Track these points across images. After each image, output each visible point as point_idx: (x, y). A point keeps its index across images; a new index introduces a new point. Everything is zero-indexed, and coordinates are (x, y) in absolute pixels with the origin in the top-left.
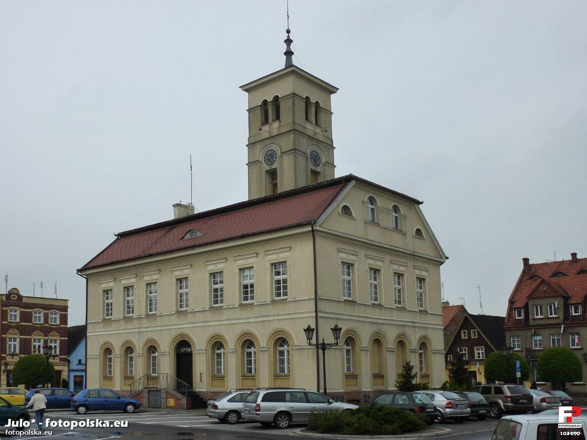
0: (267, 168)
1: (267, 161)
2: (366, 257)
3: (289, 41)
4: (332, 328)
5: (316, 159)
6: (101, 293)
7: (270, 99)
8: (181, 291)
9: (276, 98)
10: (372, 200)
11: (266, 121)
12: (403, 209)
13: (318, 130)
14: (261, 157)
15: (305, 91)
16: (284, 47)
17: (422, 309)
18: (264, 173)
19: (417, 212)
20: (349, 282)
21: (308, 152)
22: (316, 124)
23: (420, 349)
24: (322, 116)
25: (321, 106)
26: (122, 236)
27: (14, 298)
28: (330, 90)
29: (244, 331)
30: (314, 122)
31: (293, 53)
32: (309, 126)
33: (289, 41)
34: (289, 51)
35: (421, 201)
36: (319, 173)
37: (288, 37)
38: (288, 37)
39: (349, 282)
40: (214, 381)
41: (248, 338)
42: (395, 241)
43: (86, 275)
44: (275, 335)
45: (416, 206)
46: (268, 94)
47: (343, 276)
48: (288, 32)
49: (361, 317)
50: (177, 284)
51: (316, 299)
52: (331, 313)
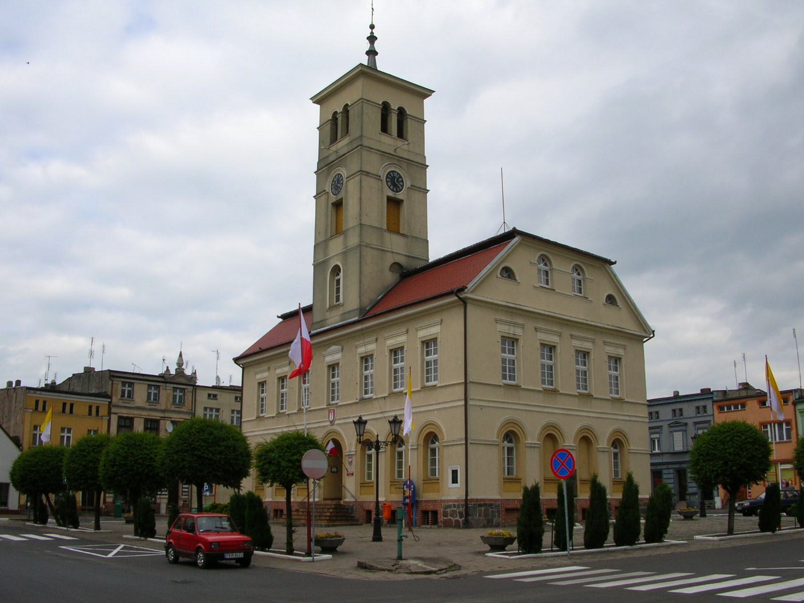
2: (497, 323)
3: (372, 39)
4: (390, 420)
5: (395, 181)
7: (340, 110)
8: (333, 380)
9: (346, 109)
10: (544, 259)
11: (334, 139)
12: (588, 273)
14: (328, 188)
16: (367, 46)
17: (617, 396)
18: (330, 205)
19: (609, 274)
20: (551, 368)
24: (410, 125)
25: (408, 113)
27: (14, 390)
29: (513, 419)
31: (376, 53)
33: (372, 39)
34: (372, 51)
35: (613, 261)
36: (402, 201)
37: (372, 33)
38: (372, 33)
39: (551, 368)
40: (299, 490)
41: (432, 430)
43: (242, 364)
44: (507, 426)
45: (607, 266)
46: (337, 106)
47: (577, 366)
48: (372, 27)
49: (484, 401)
50: (329, 371)
51: (466, 383)
52: (452, 401)
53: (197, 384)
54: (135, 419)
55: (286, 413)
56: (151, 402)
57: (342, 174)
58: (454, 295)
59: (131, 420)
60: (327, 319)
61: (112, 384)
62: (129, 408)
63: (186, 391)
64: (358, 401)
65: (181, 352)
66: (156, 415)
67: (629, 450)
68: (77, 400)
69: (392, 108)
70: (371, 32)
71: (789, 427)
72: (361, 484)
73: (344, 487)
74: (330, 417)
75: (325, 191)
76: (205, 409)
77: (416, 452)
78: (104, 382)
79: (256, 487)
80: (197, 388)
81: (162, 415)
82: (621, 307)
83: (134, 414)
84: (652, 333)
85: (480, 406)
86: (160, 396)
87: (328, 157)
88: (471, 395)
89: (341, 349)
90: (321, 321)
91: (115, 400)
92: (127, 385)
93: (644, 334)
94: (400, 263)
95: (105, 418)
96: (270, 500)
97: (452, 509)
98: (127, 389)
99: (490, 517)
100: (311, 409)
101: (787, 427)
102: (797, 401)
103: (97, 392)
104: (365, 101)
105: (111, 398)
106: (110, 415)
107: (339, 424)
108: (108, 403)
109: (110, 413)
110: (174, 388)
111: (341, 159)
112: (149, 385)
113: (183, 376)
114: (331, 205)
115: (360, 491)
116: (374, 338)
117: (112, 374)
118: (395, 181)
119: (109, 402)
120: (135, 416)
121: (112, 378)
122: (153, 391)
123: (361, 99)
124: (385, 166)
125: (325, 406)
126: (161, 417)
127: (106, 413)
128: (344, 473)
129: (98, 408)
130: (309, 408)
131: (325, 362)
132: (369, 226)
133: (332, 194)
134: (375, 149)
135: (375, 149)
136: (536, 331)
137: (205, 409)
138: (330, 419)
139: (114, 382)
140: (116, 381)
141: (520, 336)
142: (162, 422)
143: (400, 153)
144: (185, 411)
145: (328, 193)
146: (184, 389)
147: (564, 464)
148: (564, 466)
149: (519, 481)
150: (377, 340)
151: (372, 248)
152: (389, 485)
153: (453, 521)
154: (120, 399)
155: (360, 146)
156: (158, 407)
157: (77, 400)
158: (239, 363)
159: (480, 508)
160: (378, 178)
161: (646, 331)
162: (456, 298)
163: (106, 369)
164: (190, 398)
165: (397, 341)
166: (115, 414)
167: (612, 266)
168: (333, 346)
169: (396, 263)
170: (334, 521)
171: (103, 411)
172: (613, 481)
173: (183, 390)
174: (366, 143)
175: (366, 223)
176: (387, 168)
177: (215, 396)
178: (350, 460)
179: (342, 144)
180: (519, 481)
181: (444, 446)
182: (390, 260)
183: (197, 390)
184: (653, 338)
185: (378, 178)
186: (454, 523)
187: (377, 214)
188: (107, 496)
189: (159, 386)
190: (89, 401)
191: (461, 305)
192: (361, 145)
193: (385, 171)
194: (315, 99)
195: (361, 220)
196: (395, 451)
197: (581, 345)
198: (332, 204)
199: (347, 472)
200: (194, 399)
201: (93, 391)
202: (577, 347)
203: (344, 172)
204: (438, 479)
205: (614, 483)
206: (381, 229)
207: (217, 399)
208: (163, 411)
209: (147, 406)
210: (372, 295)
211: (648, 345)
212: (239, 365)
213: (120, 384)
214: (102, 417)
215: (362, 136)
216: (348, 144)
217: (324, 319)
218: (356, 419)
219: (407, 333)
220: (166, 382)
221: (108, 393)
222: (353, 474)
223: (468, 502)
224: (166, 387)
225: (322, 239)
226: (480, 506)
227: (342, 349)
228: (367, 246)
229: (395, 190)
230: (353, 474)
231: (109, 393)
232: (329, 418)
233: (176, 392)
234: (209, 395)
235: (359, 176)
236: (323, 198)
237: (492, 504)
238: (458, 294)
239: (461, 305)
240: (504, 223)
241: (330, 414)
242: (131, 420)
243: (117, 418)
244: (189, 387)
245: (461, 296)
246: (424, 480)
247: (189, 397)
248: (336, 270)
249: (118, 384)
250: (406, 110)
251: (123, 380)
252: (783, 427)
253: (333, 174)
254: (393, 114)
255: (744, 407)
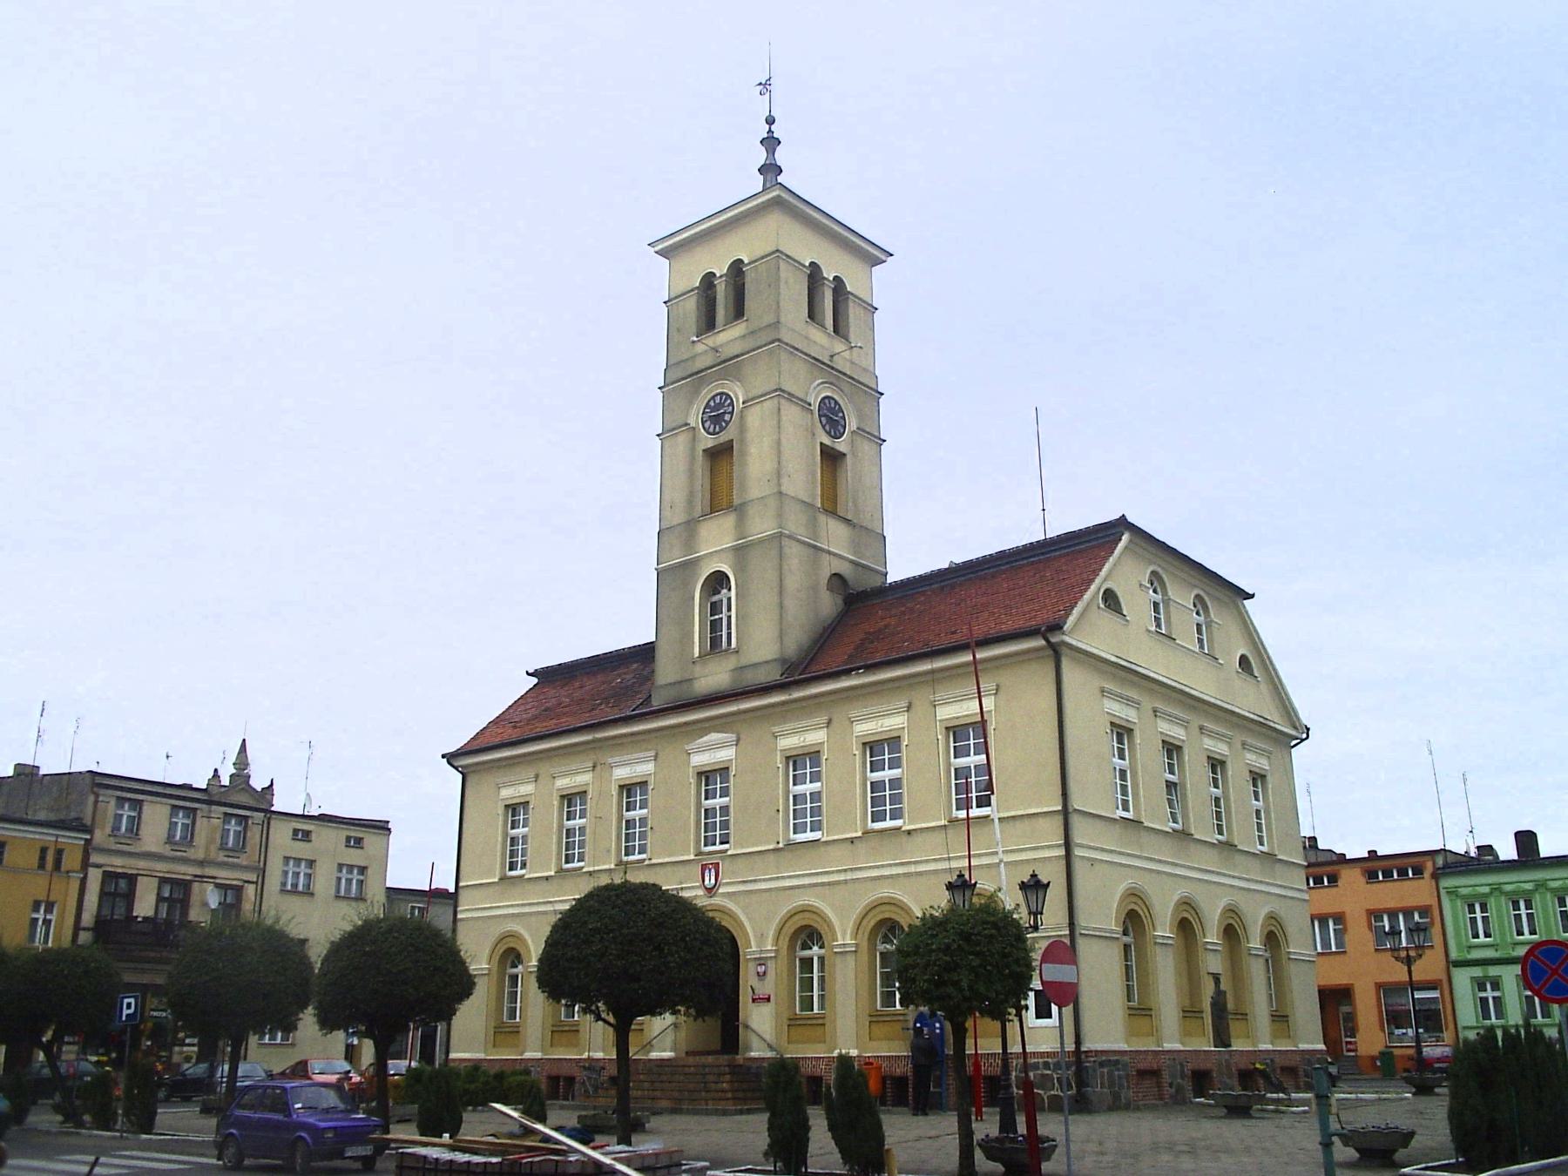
0: (709, 441)
1: (709, 423)
3: (771, 142)
5: (831, 417)
6: (615, 792)
7: (721, 269)
9: (737, 268)
11: (708, 323)
13: (839, 346)
14: (695, 418)
15: (807, 249)
21: (814, 400)
22: (836, 330)
23: (1125, 933)
24: (854, 313)
25: (849, 289)
26: (547, 677)
28: (871, 255)
30: (829, 322)
32: (816, 335)
33: (771, 142)
37: (770, 131)
38: (770, 131)
42: (1202, 683)
48: (770, 121)
51: (1066, 812)
53: (273, 809)
54: (139, 878)
55: (584, 870)
56: (176, 844)
57: (731, 393)
58: (1041, 638)
59: (132, 879)
60: (696, 679)
61: (96, 802)
62: (130, 854)
63: (250, 822)
64: (781, 845)
65: (244, 740)
66: (186, 871)
67: (1289, 953)
68: (14, 834)
69: (825, 275)
70: (768, 130)
71: (1340, 927)
72: (790, 1019)
73: (747, 1027)
74: (707, 879)
75: (687, 424)
76: (287, 859)
77: (854, 958)
78: (74, 797)
79: (495, 1027)
80: (274, 816)
81: (198, 872)
82: (1259, 679)
83: (138, 869)
84: (1306, 731)
85: (1088, 859)
86: (196, 832)
87: (693, 358)
88: (1077, 838)
89: (735, 739)
90: (680, 682)
91: (100, 836)
92: (127, 806)
93: (1294, 733)
94: (841, 573)
95: (74, 874)
96: (538, 1055)
97: (1039, 1072)
98: (127, 812)
99: (1117, 1089)
100: (654, 861)
101: (1337, 927)
102: (1439, 872)
103: (52, 817)
104: (784, 257)
105: (89, 830)
106: (87, 869)
107: (729, 895)
108: (83, 842)
109: (86, 864)
110: (226, 814)
111: (728, 366)
112: (174, 807)
113: (247, 791)
114: (701, 452)
115: (788, 1032)
116: (824, 719)
117: (98, 780)
118: (831, 417)
119: (86, 840)
120: (141, 872)
121: (95, 789)
122: (181, 820)
123: (777, 251)
124: (818, 385)
125: (692, 857)
126: (196, 876)
127: (77, 865)
128: (745, 997)
129: (59, 853)
130: (650, 859)
131: (692, 765)
132: (793, 497)
133: (702, 430)
134: (802, 352)
135: (802, 352)
136: (1156, 716)
137: (287, 859)
138: (707, 882)
139: (101, 799)
140: (103, 795)
141: (1135, 723)
142: (196, 886)
143: (839, 363)
144: (245, 863)
145: (694, 428)
146: (246, 818)
147: (1550, 972)
148: (1551, 969)
149: (1148, 1013)
150: (829, 722)
151: (798, 541)
152: (492, 1033)
153: (1045, 1098)
154: (109, 835)
155: (773, 340)
156: (191, 854)
157: (14, 834)
158: (456, 764)
159: (1101, 1070)
160: (805, 405)
161: (1295, 728)
162: (1043, 642)
163: (84, 769)
164: (258, 836)
165: (882, 727)
166: (98, 866)
167: (1246, 602)
168: (713, 734)
169: (837, 577)
170: (745, 1100)
171: (72, 860)
172: (1272, 1016)
173: (243, 820)
174: (786, 337)
175: (789, 493)
176: (819, 391)
177: (307, 834)
178: (761, 969)
179: (729, 336)
180: (1148, 1013)
181: (836, 952)
182: (829, 567)
183: (272, 822)
184: (1306, 741)
185: (805, 405)
186: (1046, 1101)
187: (802, 479)
188: (64, 1049)
189: (195, 810)
190: (41, 837)
191: (1048, 656)
192: (779, 340)
193: (816, 397)
194: (660, 247)
195: (779, 485)
196: (796, 957)
197: (1214, 747)
198: (704, 451)
199: (754, 992)
200: (264, 836)
201: (42, 816)
202: (1211, 751)
203: (738, 394)
204: (642, 1024)
205: (1276, 1019)
206: (811, 506)
207: (310, 841)
208: (201, 863)
209: (166, 850)
210: (796, 640)
211: (1299, 754)
212: (456, 768)
213: (113, 802)
214: (68, 872)
215: (778, 322)
216: (744, 336)
217: (687, 676)
218: (953, 878)
219: (908, 711)
220: (210, 803)
221: (84, 822)
222: (768, 1000)
223: (1083, 1056)
224: (210, 811)
225: (678, 517)
226: (1102, 1064)
227: (738, 740)
228: (790, 537)
229: (833, 433)
230: (768, 1000)
231: (88, 821)
232: (703, 881)
233: (229, 823)
234: (296, 831)
235: (776, 400)
236: (683, 439)
237: (1117, 1062)
238: (1048, 635)
239: (1048, 656)
240: (1044, 510)
241: (707, 874)
242: (132, 879)
243: (100, 877)
244: (256, 814)
245: (1053, 640)
246: (553, 1026)
247: (254, 835)
248: (718, 581)
249: (108, 802)
250: (847, 284)
251: (119, 793)
252: (1328, 925)
253: (706, 394)
254: (826, 288)
255: (1336, 882)
